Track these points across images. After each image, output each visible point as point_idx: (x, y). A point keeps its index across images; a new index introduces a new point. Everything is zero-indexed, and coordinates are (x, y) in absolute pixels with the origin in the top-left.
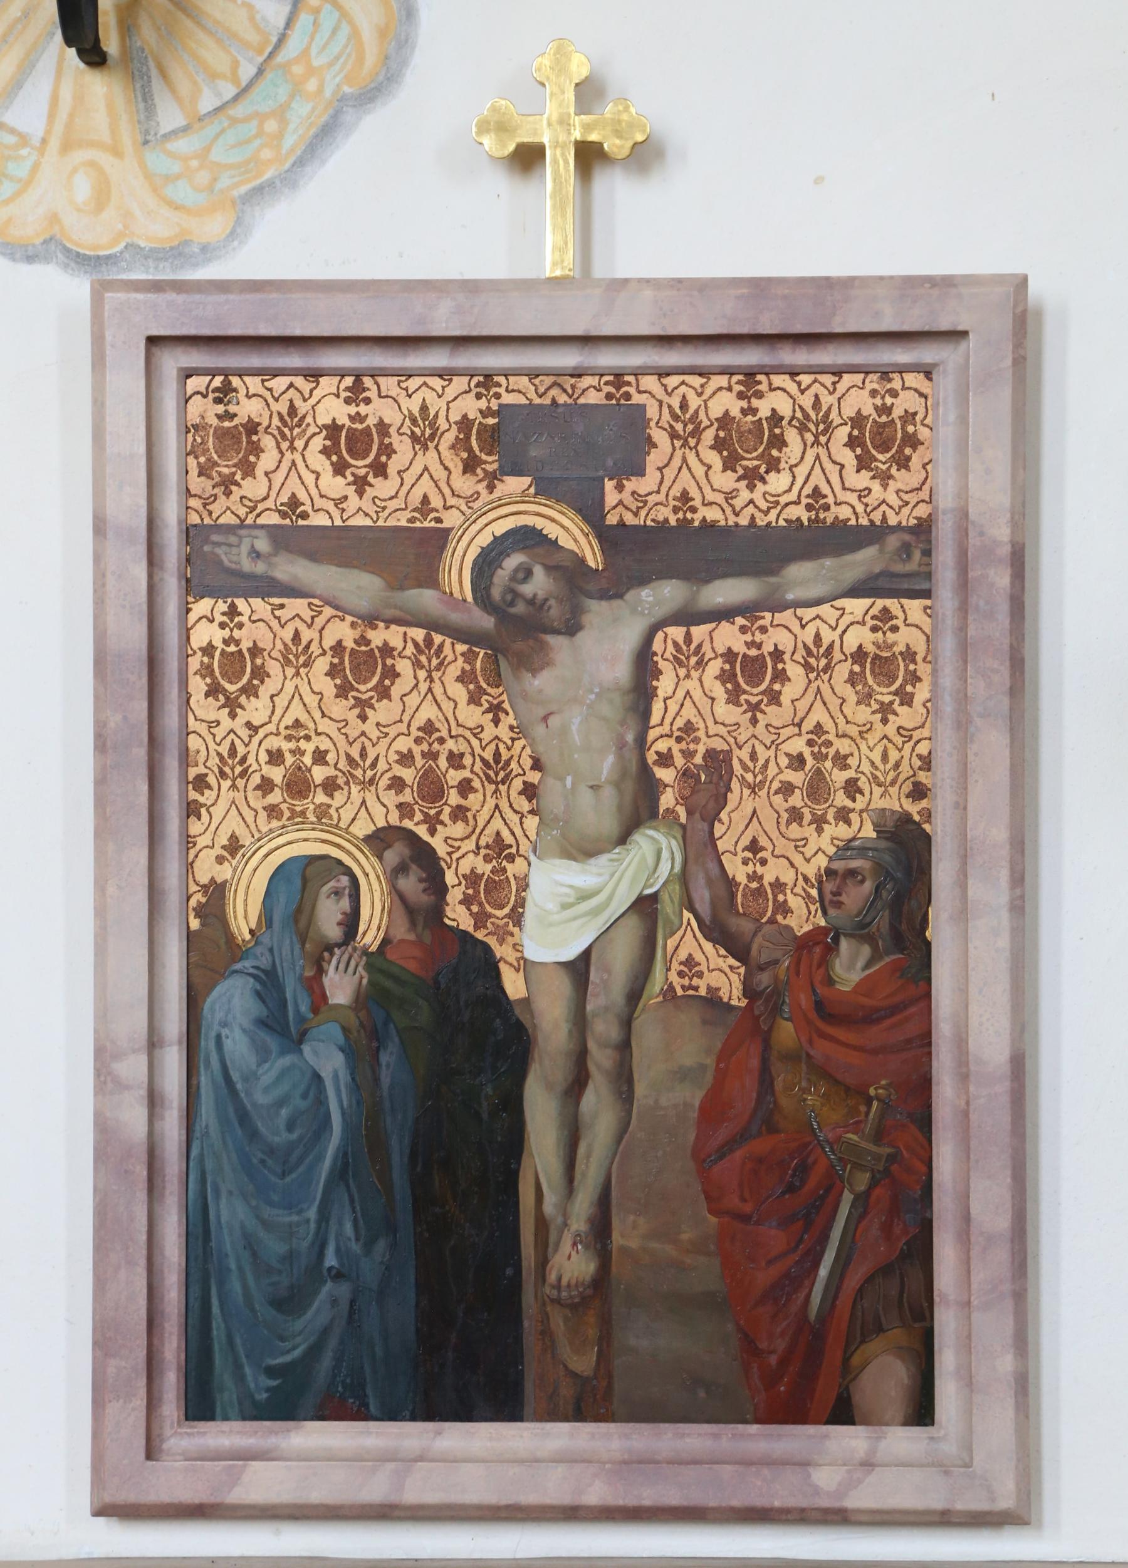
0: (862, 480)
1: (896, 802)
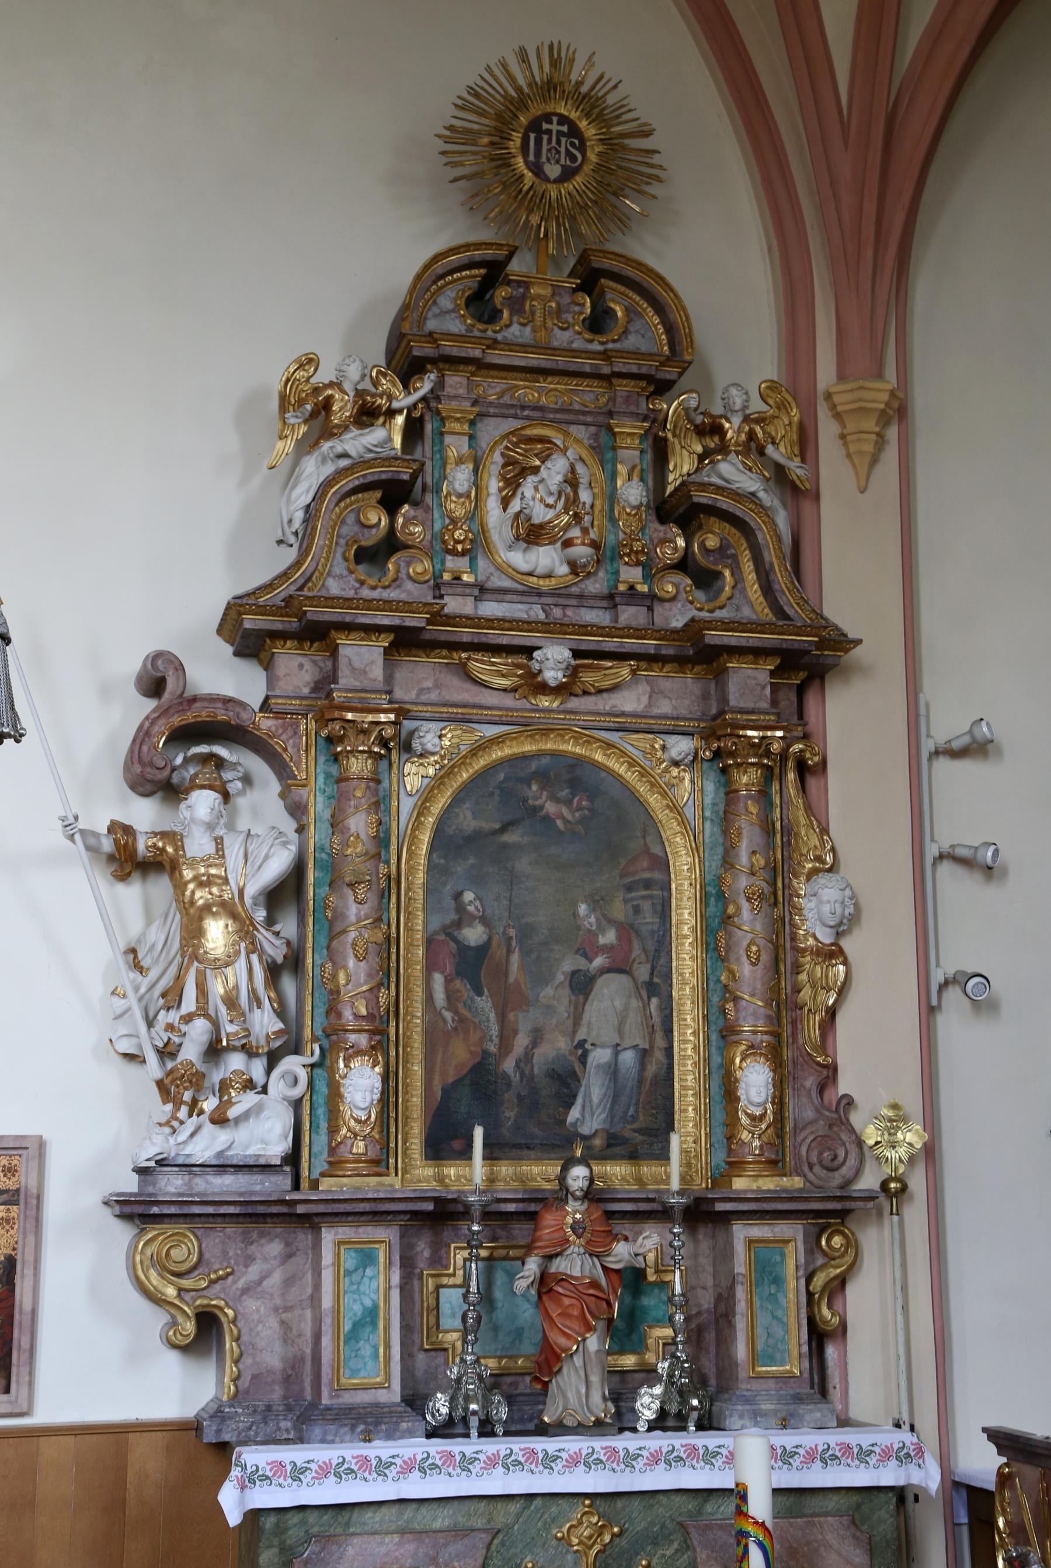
0: (5, 1179)
1: (9, 1251)
